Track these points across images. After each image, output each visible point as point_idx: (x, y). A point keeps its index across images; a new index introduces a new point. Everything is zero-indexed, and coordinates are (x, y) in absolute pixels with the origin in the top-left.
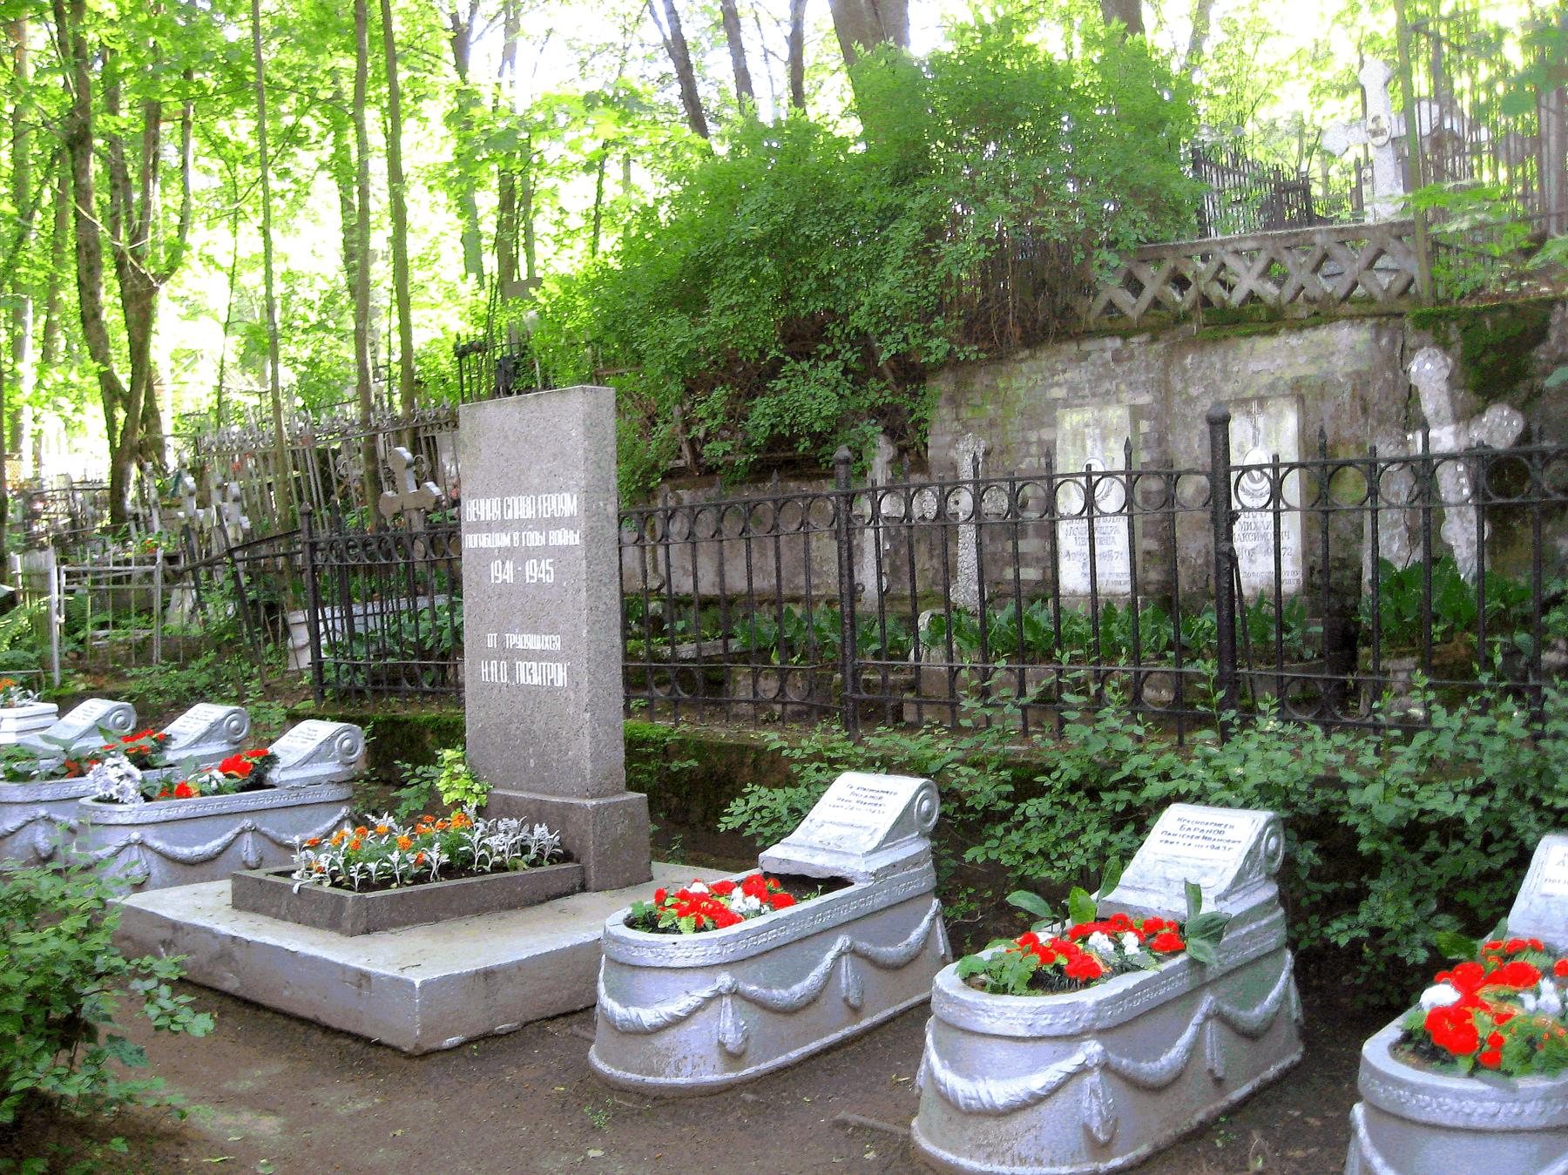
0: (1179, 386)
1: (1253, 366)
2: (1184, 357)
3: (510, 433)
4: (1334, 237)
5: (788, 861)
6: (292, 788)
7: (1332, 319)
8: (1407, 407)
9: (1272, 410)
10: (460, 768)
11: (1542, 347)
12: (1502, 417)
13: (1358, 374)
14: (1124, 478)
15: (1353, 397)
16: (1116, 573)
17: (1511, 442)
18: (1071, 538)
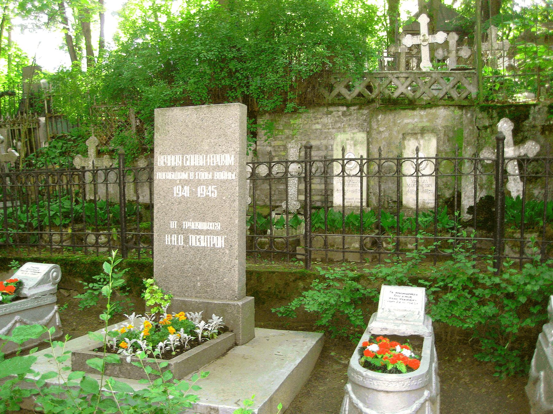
0: (375, 127)
1: (406, 121)
2: (377, 115)
3: (190, 124)
4: (440, 76)
5: (386, 329)
6: (36, 298)
7: (436, 106)
8: (478, 140)
9: (426, 138)
10: (155, 287)
11: (527, 121)
12: (532, 145)
13: (447, 126)
14: (434, 160)
15: (445, 135)
16: (428, 198)
17: (535, 154)
18: (408, 183)
